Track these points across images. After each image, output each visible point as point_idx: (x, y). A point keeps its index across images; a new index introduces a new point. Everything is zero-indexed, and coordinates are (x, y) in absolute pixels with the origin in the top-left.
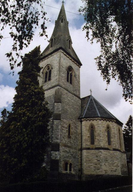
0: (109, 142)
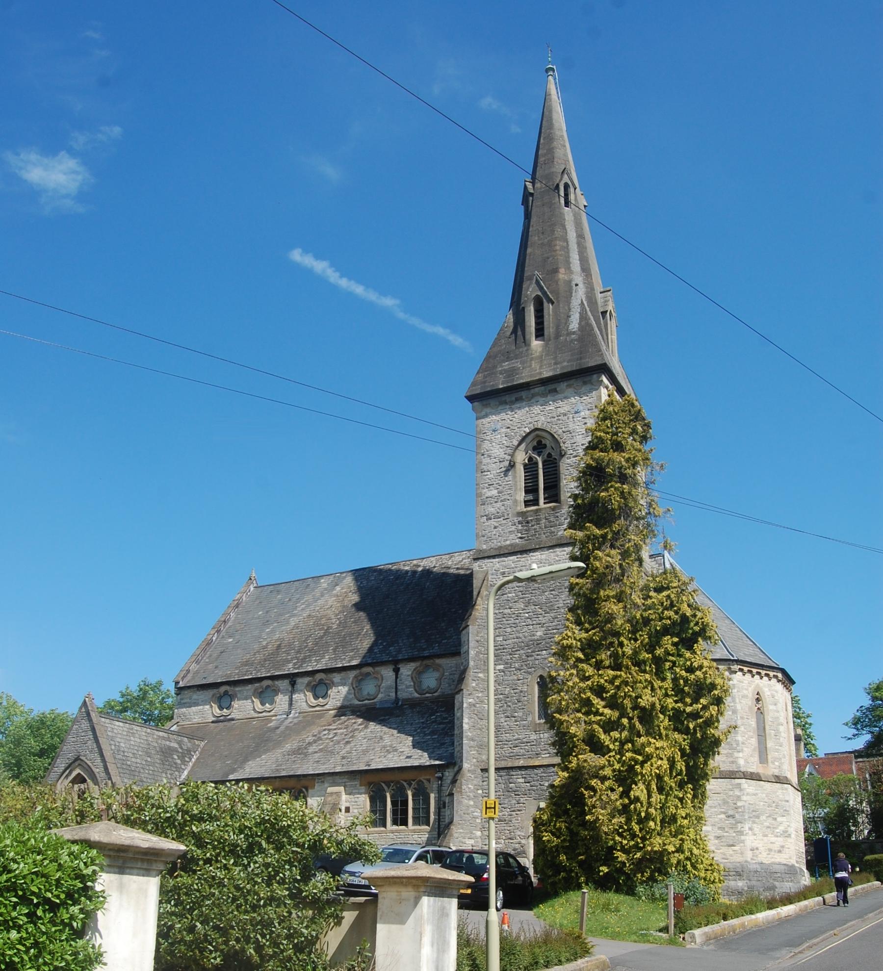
0: (763, 754)
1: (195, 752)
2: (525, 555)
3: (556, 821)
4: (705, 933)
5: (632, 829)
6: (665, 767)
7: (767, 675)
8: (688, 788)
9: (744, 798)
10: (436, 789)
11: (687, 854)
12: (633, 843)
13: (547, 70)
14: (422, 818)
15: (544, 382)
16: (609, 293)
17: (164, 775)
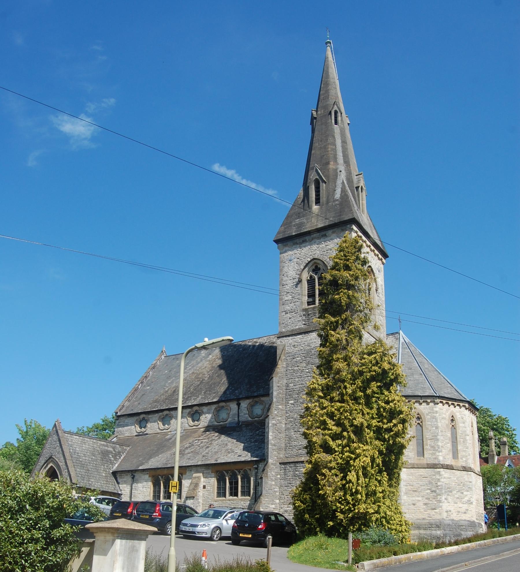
0: (455, 454)
1: (123, 453)
2: (307, 335)
3: (304, 494)
4: (373, 564)
5: (347, 499)
6: (367, 461)
7: (458, 405)
8: (383, 474)
9: (442, 480)
11: (382, 514)
12: (347, 507)
13: (327, 43)
14: (246, 492)
15: (319, 230)
16: (361, 175)
17: (102, 467)
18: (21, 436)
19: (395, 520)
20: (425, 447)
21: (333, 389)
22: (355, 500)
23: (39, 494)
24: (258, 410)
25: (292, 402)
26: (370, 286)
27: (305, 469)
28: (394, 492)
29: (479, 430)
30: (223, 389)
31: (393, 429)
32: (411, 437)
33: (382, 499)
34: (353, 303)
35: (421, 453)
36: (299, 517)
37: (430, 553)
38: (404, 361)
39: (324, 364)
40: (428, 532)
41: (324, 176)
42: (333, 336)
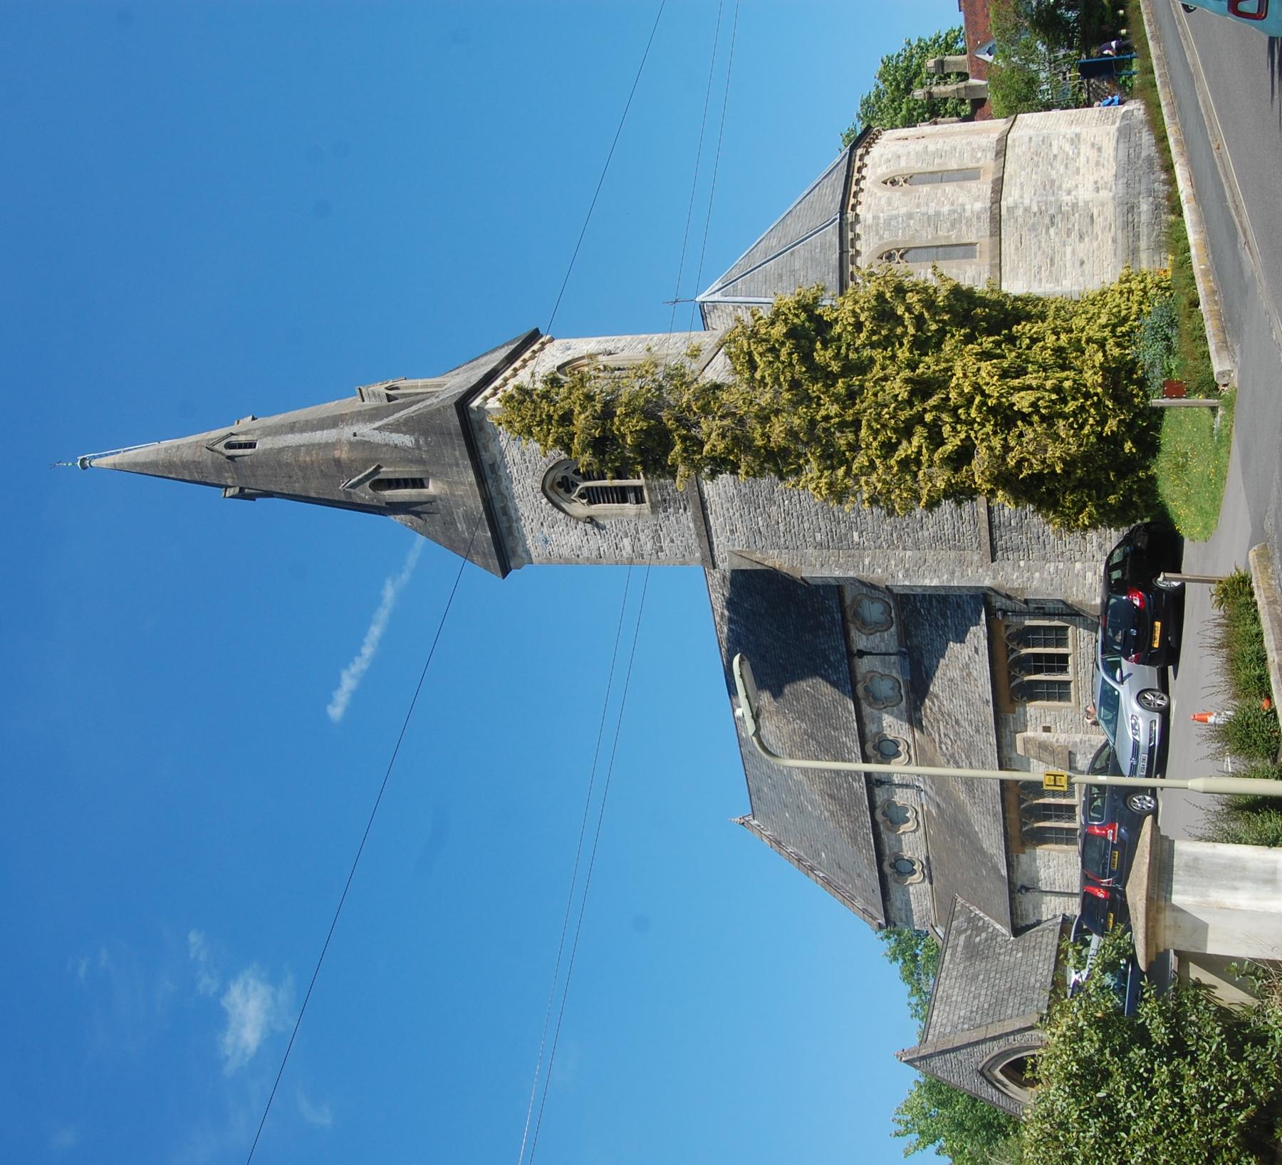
1: (971, 911)
2: (708, 504)
3: (1064, 507)
4: (1217, 352)
5: (1073, 411)
6: (989, 368)
7: (860, 170)
8: (1018, 332)
9: (1027, 202)
10: (1019, 618)
11: (1107, 333)
12: (1092, 410)
13: (84, 467)
14: (1059, 637)
15: (481, 480)
16: (363, 391)
17: (1002, 958)
18: (930, 1146)
19: (1118, 306)
20: (954, 242)
21: (830, 444)
22: (1075, 393)
23: (1074, 1069)
24: (874, 611)
25: (856, 535)
26: (602, 367)
27: (1007, 504)
28: (1056, 307)
29: (909, 122)
30: (826, 689)
31: (916, 313)
32: (935, 274)
33: (1073, 335)
34: (642, 404)
35: (966, 249)
36: (1114, 516)
37: (1192, 226)
38: (763, 291)
39: (776, 464)
40: (1144, 230)
41: (366, 469)
42: (714, 446)
